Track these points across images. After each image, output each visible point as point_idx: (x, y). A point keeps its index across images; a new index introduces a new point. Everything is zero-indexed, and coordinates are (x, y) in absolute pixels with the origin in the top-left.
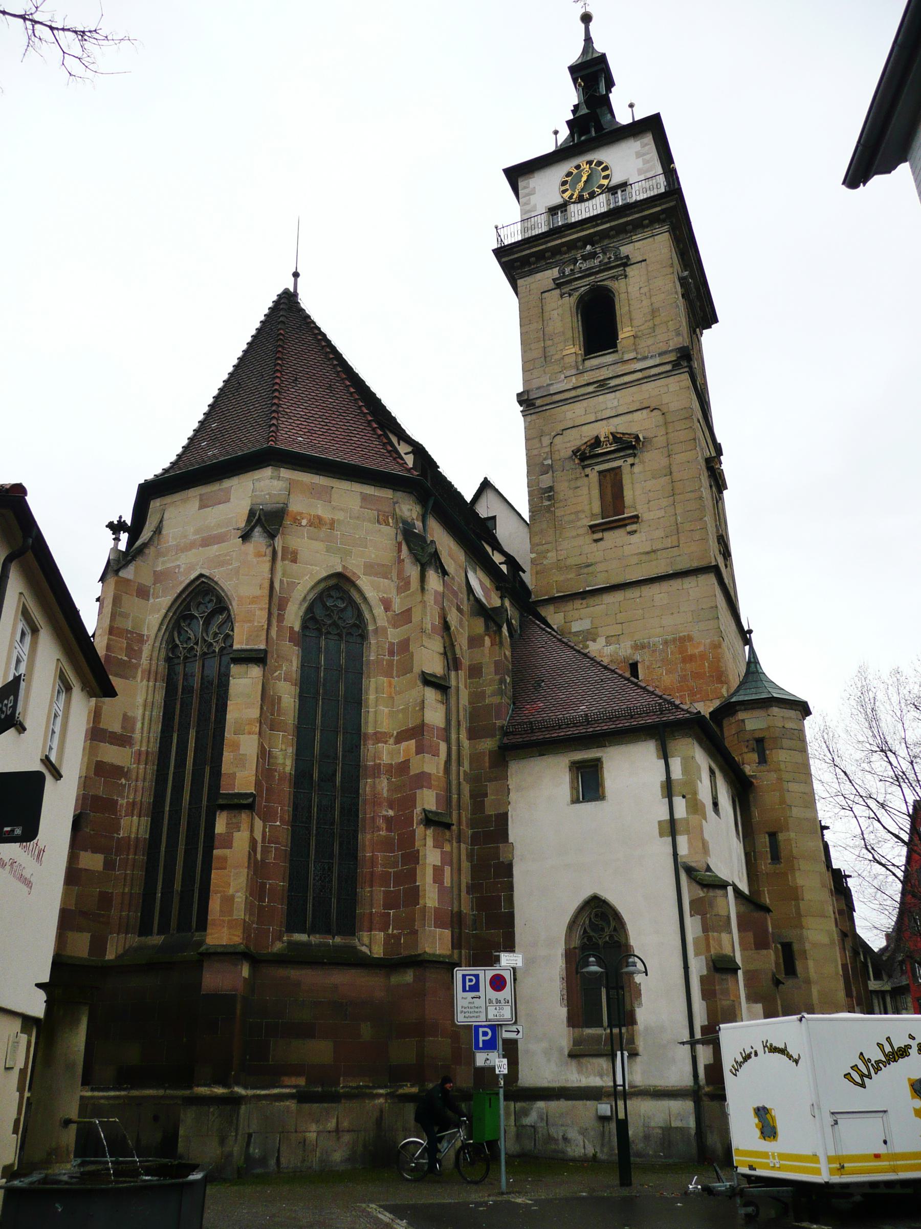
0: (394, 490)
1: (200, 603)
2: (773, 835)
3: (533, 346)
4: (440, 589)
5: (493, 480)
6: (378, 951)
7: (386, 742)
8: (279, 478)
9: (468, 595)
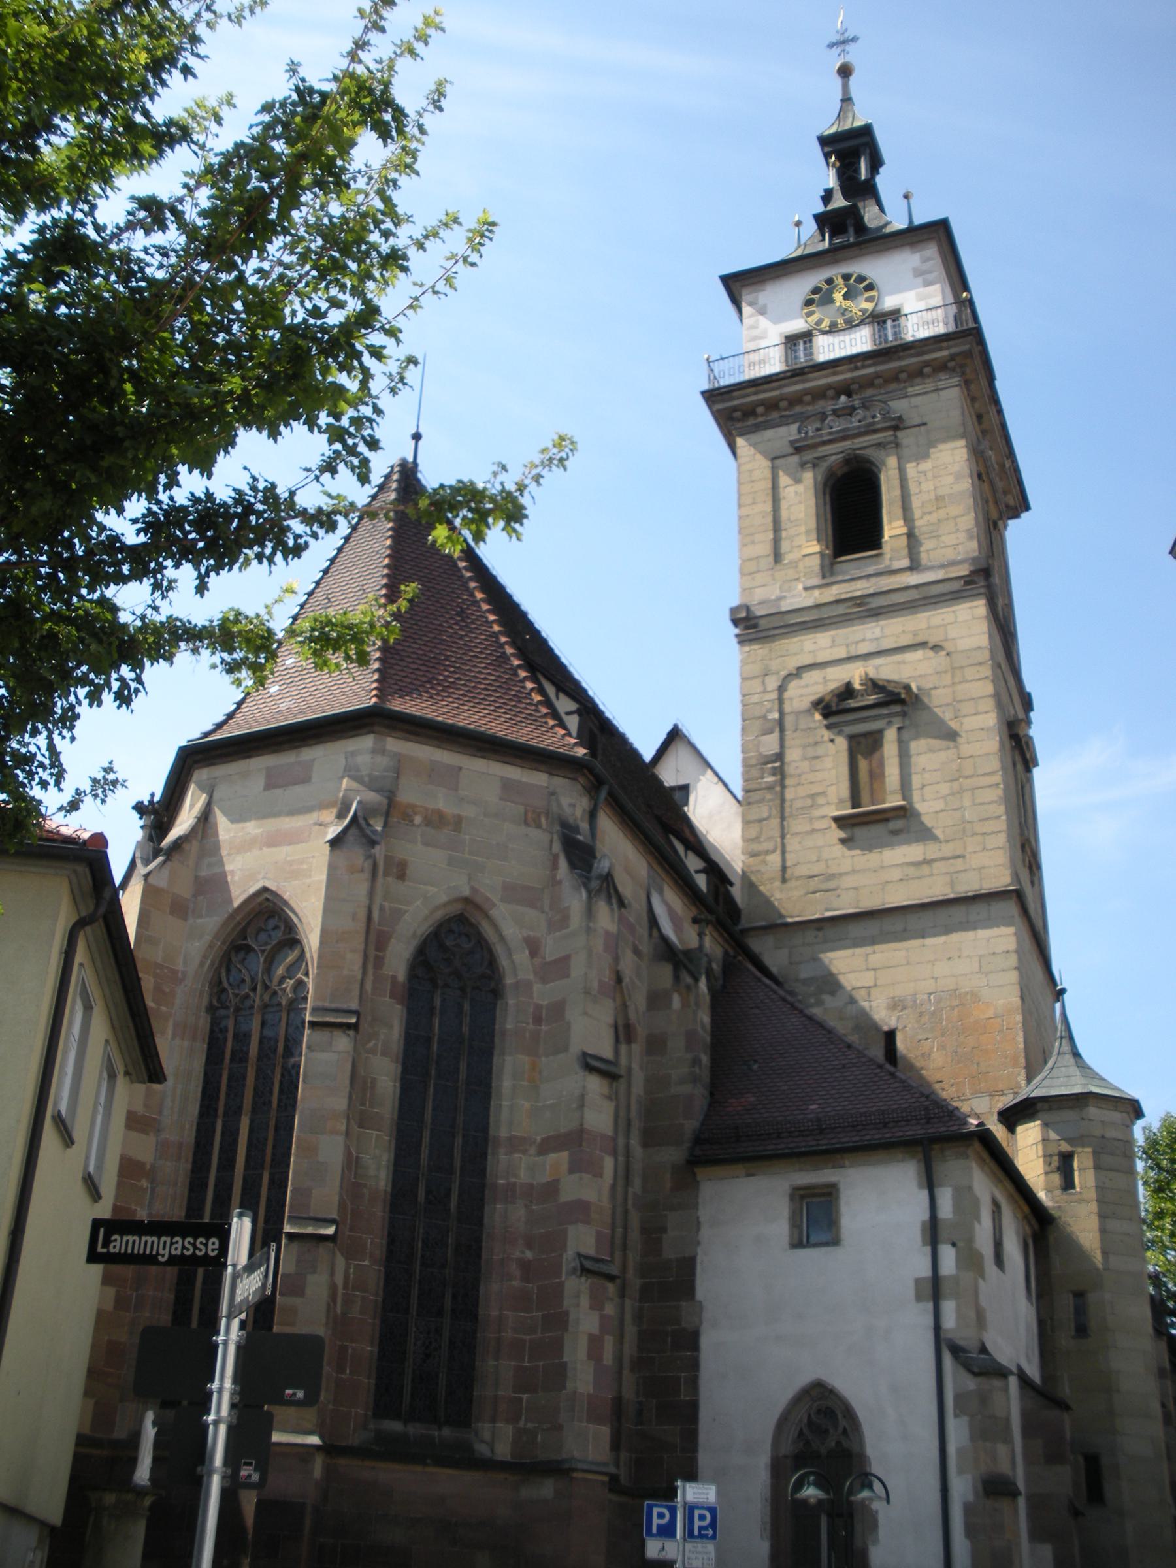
0: (551, 774)
1: (261, 930)
2: (1079, 1295)
3: (757, 537)
4: (613, 928)
5: (688, 729)
6: (503, 1451)
7: (525, 1152)
8: (383, 752)
9: (651, 929)
